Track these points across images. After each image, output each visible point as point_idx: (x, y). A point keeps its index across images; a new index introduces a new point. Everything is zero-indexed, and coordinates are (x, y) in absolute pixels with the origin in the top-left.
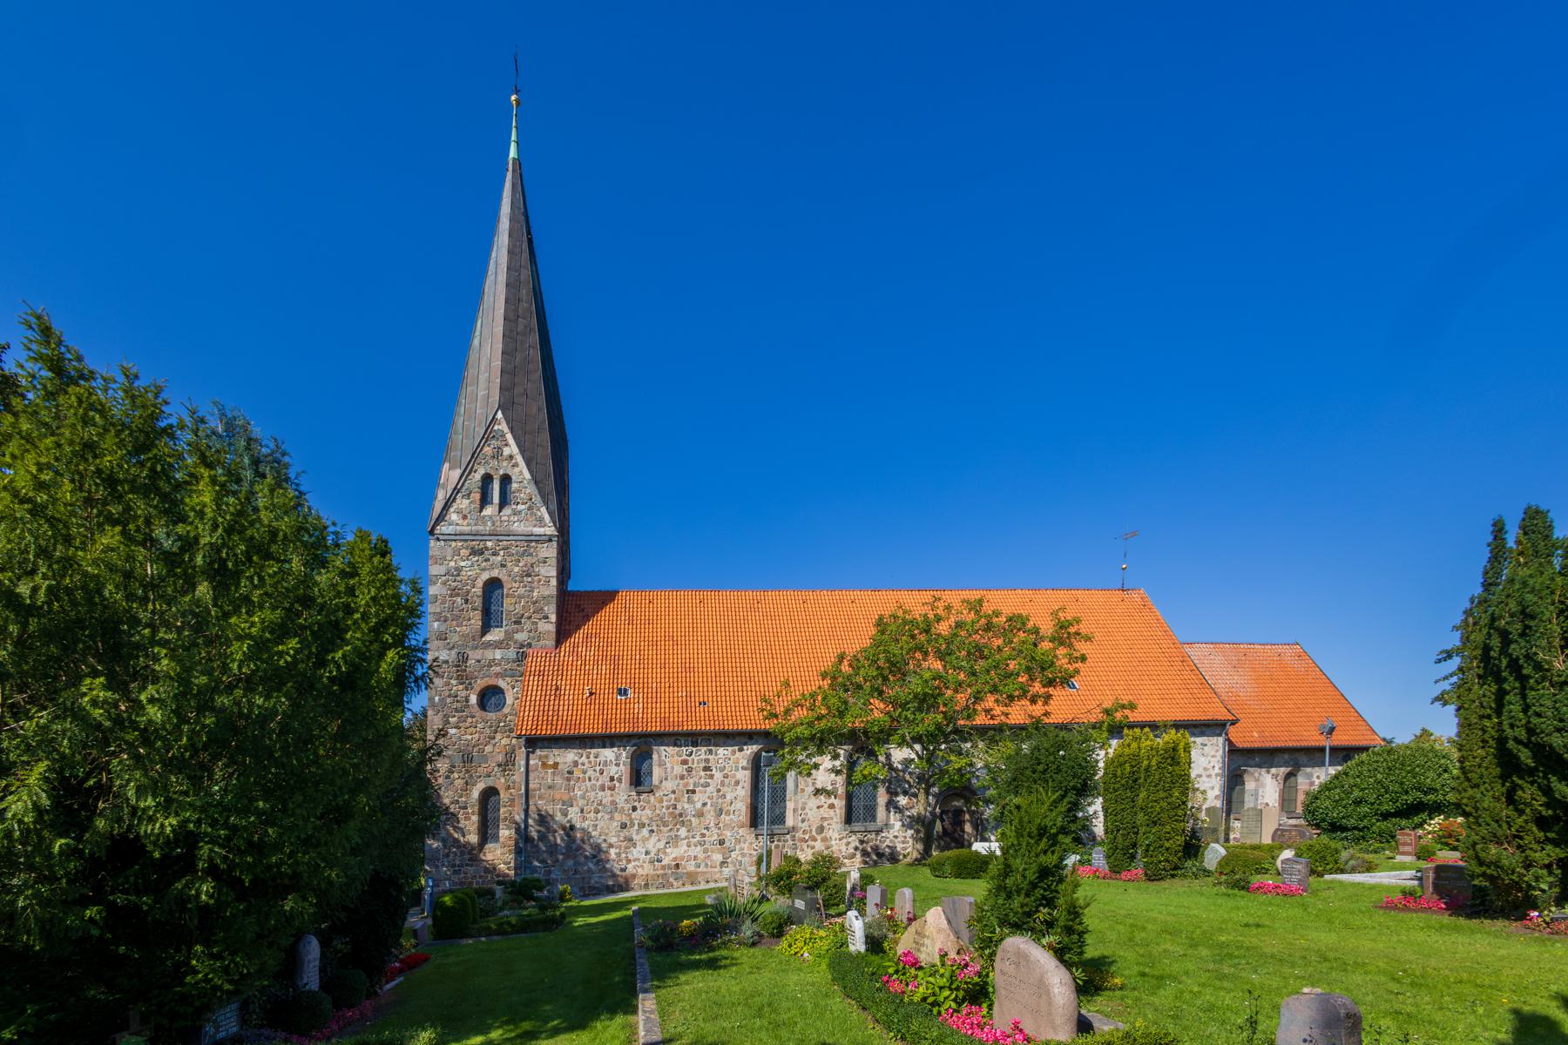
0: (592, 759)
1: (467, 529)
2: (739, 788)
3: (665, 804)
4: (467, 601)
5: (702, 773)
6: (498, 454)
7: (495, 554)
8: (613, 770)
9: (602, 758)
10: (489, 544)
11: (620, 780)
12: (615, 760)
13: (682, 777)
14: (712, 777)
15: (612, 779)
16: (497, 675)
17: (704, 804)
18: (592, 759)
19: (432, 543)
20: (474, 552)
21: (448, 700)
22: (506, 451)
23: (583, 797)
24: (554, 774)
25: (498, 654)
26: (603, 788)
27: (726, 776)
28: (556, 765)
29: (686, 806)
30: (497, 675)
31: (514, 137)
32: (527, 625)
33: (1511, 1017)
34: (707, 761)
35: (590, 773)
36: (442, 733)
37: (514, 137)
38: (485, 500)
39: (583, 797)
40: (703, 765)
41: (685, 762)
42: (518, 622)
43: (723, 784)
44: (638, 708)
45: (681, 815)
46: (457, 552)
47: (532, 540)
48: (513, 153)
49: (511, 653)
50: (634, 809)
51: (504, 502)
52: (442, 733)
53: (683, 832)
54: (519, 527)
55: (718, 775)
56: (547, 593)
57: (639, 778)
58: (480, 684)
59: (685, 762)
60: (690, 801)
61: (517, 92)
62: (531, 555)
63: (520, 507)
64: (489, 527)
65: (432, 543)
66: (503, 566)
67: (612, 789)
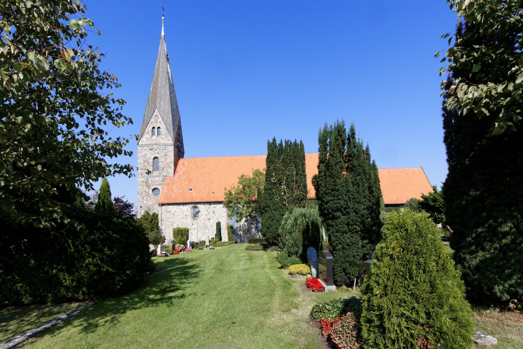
0: (180, 210)
1: (148, 143)
2: (223, 218)
3: (201, 223)
4: (148, 164)
5: (212, 214)
6: (156, 121)
7: (156, 150)
8: (186, 213)
9: (183, 209)
10: (154, 147)
11: (188, 216)
12: (187, 209)
13: (206, 215)
14: (215, 215)
15: (186, 215)
16: (157, 185)
17: (213, 223)
18: (180, 210)
19: (138, 147)
20: (150, 150)
21: (144, 192)
22: (159, 120)
23: (177, 221)
24: (169, 214)
25: (157, 179)
26: (183, 218)
27: (219, 215)
28: (170, 212)
29: (208, 223)
30: (157, 185)
31: (163, 25)
32: (165, 170)
33: (269, 250)
34: (214, 210)
35: (180, 214)
36: (244, 206)
37: (163, 25)
38: (153, 134)
39: (177, 221)
40: (212, 211)
41: (207, 211)
42: (163, 169)
43: (218, 217)
44: (194, 194)
45: (206, 226)
46: (145, 150)
47: (166, 145)
48: (163, 33)
49: (161, 178)
50: (192, 224)
51: (158, 134)
52: (244, 206)
53: (207, 231)
54: (163, 142)
55: (217, 214)
56: (171, 161)
57: (195, 215)
58: (153, 188)
59: (207, 211)
60: (209, 222)
61: (163, 16)
62: (166, 150)
63: (163, 136)
64: (154, 142)
65: (138, 147)
66: (158, 153)
67: (186, 218)
